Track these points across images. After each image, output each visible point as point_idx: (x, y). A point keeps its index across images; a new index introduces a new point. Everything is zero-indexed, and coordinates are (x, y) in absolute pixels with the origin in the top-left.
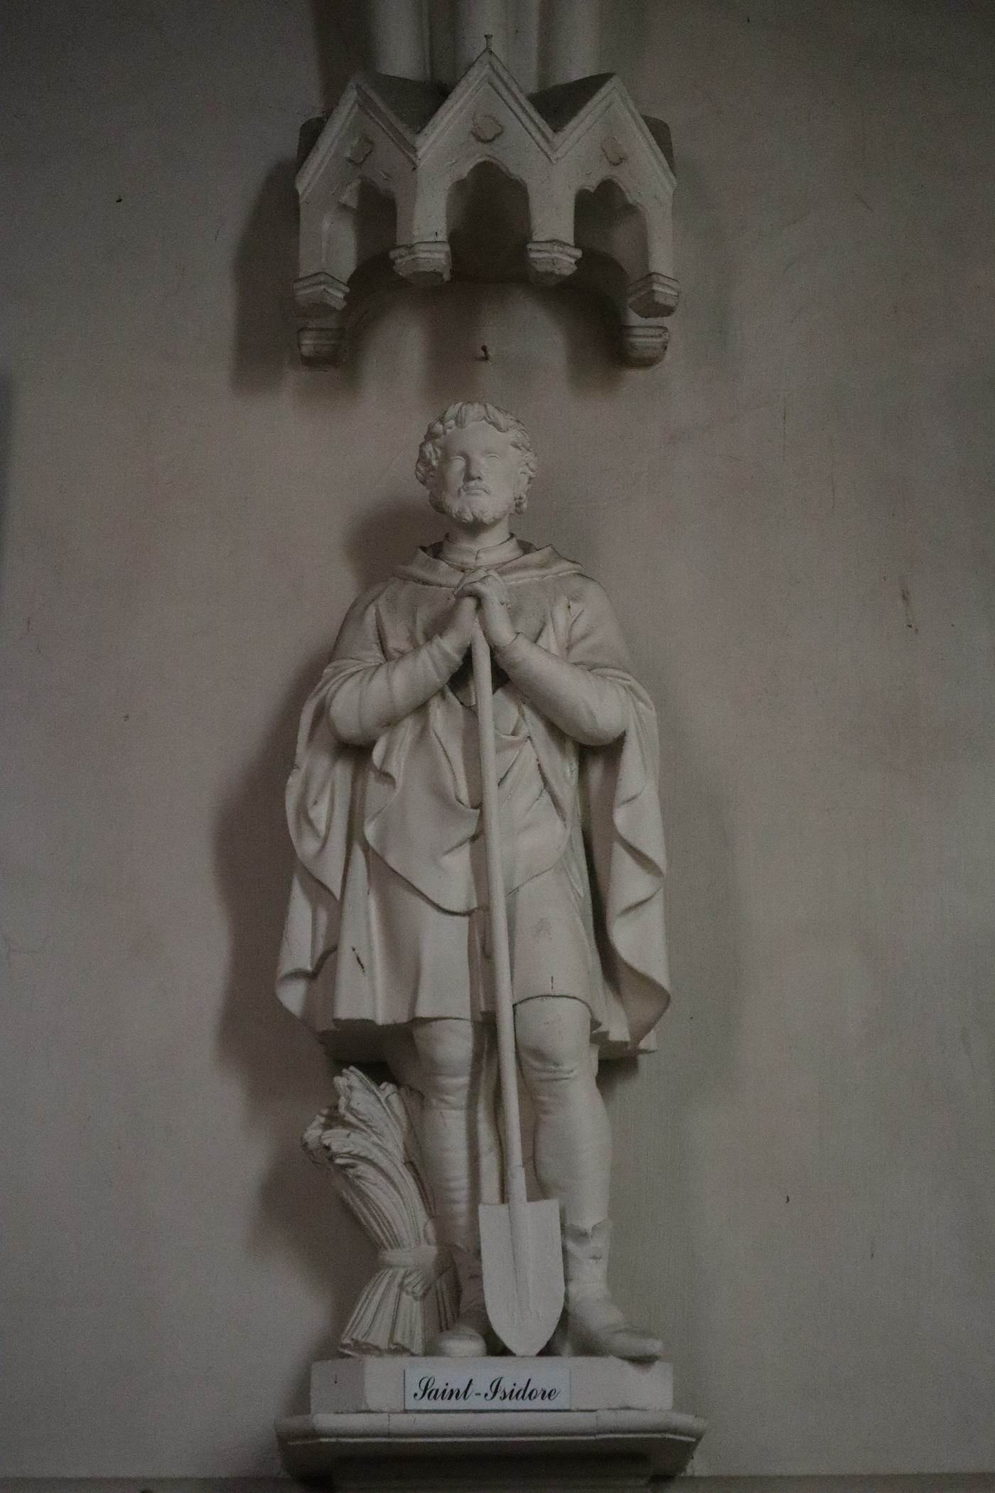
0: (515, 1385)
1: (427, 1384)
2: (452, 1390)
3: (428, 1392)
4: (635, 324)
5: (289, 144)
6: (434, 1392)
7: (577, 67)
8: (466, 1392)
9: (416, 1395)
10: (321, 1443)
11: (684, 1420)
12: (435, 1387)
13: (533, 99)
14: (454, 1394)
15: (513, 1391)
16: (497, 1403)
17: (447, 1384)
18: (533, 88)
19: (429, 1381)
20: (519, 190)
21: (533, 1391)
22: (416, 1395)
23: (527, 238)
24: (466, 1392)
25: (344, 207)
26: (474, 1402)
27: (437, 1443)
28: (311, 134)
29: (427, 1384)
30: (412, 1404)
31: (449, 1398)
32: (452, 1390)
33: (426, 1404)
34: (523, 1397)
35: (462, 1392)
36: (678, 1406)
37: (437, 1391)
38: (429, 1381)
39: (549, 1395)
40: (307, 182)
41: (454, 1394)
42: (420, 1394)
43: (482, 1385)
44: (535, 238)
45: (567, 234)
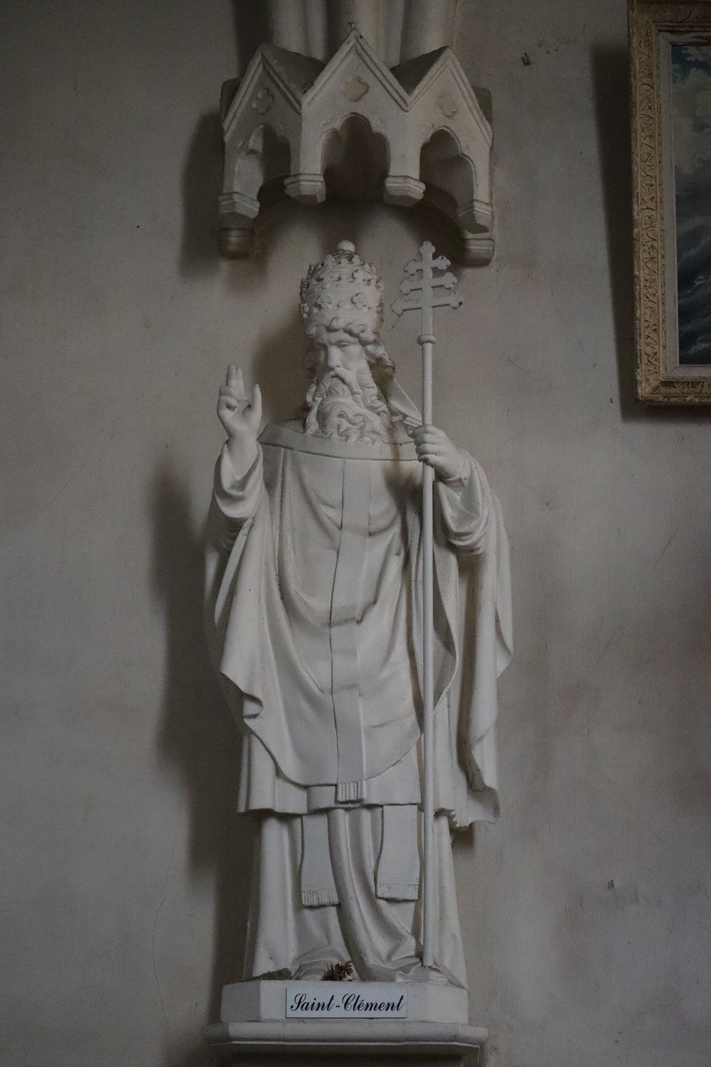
0: (315, 999)
1: (301, 999)
2: (319, 1004)
3: (301, 1004)
4: (478, 198)
5: (214, 100)
6: (305, 1005)
7: (431, 44)
8: (399, 1005)
9: (292, 1007)
10: (232, 1044)
11: (479, 1032)
12: (306, 1001)
13: (393, 70)
14: (321, 1006)
15: (314, 1003)
16: (351, 1013)
17: (315, 999)
18: (395, 60)
19: (301, 997)
20: (381, 142)
21: (361, 1004)
22: (292, 1007)
23: (385, 174)
24: (399, 1005)
25: (252, 152)
26: (334, 1012)
27: (321, 1046)
28: (231, 90)
29: (301, 999)
30: (291, 1014)
31: (317, 1010)
32: (319, 1004)
33: (300, 1013)
34: (306, 1009)
35: (396, 1004)
36: (471, 1022)
37: (308, 1004)
38: (301, 997)
39: (380, 1007)
40: (230, 126)
41: (321, 1006)
42: (295, 1006)
43: (338, 1001)
44: (390, 174)
45: (416, 174)
